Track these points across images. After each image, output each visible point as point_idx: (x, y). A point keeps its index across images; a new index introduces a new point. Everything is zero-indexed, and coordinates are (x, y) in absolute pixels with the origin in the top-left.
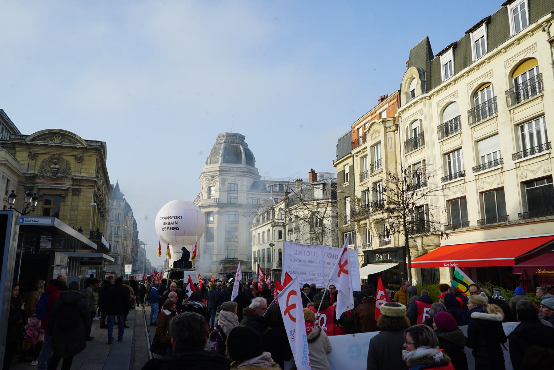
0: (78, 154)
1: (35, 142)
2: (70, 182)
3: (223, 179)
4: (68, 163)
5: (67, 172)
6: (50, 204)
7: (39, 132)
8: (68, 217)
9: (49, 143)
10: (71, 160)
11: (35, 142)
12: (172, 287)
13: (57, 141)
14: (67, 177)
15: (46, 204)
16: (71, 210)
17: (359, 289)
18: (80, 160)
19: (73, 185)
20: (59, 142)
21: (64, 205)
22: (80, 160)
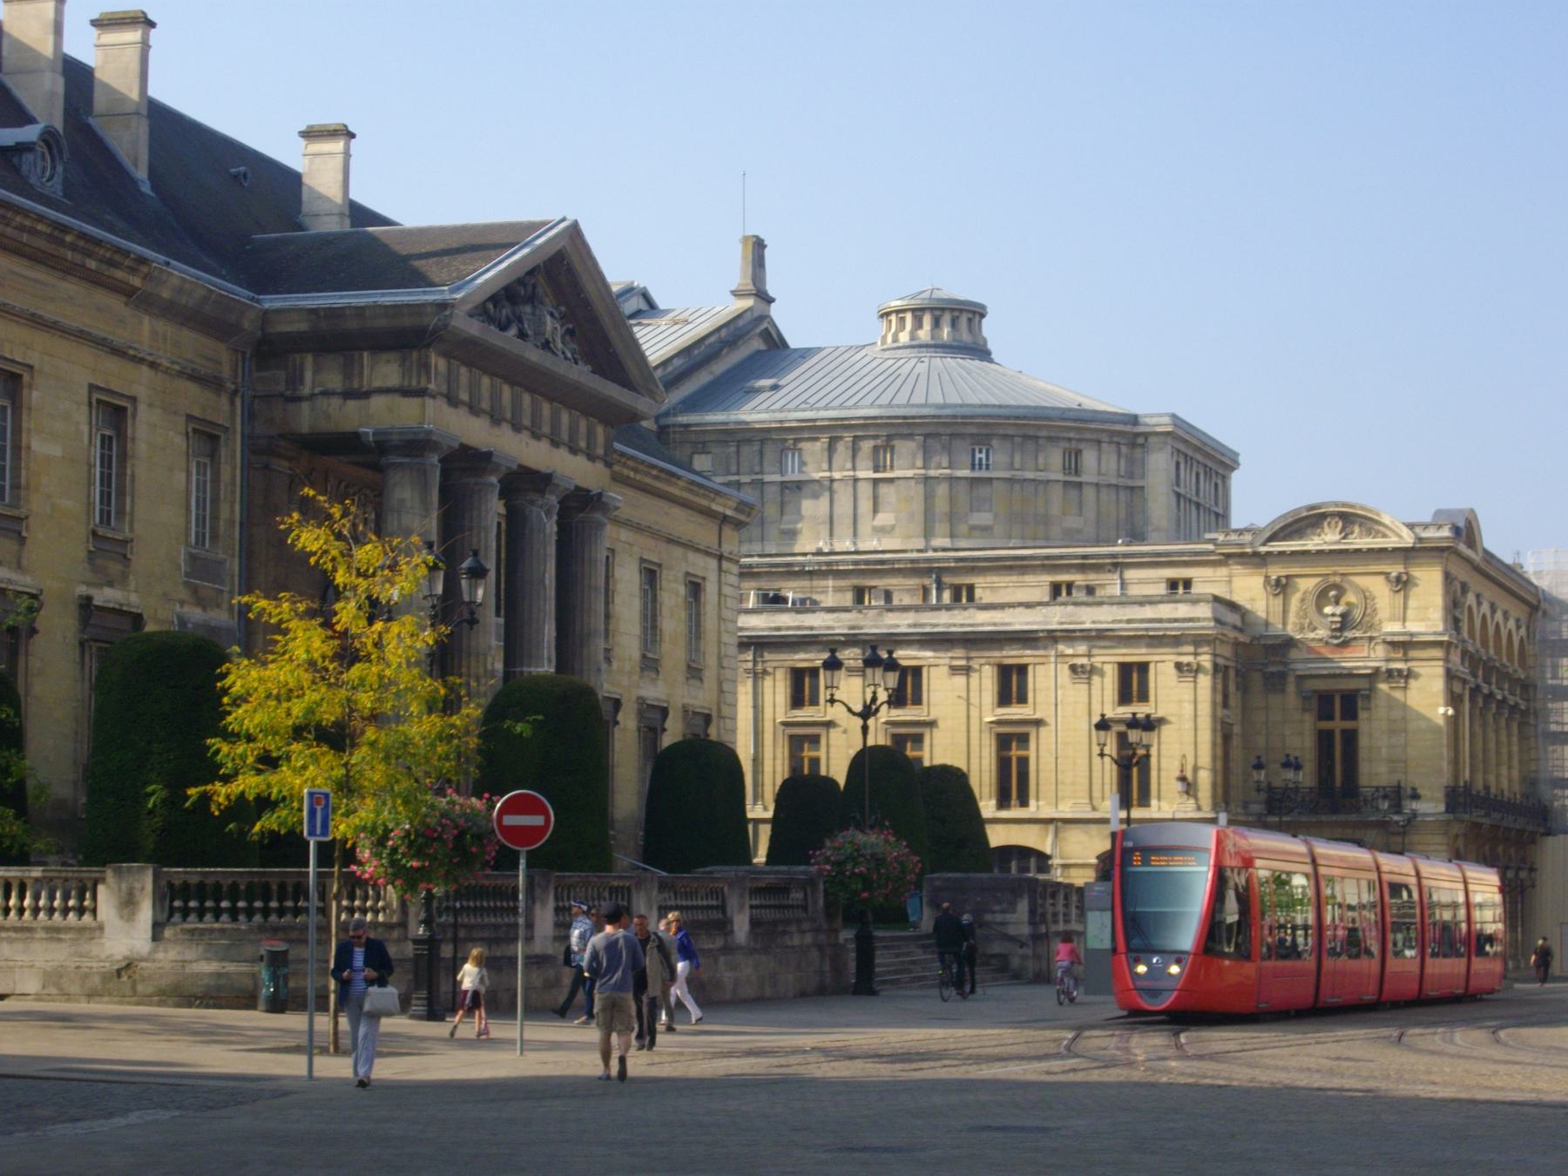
0: (1395, 569)
1: (1277, 546)
2: (1380, 651)
3: (1077, 472)
4: (1366, 597)
5: (1368, 621)
6: (1343, 718)
7: (1284, 516)
8: (1384, 751)
9: (1312, 543)
10: (1379, 588)
11: (1277, 546)
12: (928, 534)
13: (1328, 538)
14: (1371, 639)
15: (1320, 718)
16: (1392, 732)
17: (589, 368)
18: (1402, 584)
19: (1388, 660)
20: (1337, 537)
21: (1369, 719)
22: (1402, 584)
